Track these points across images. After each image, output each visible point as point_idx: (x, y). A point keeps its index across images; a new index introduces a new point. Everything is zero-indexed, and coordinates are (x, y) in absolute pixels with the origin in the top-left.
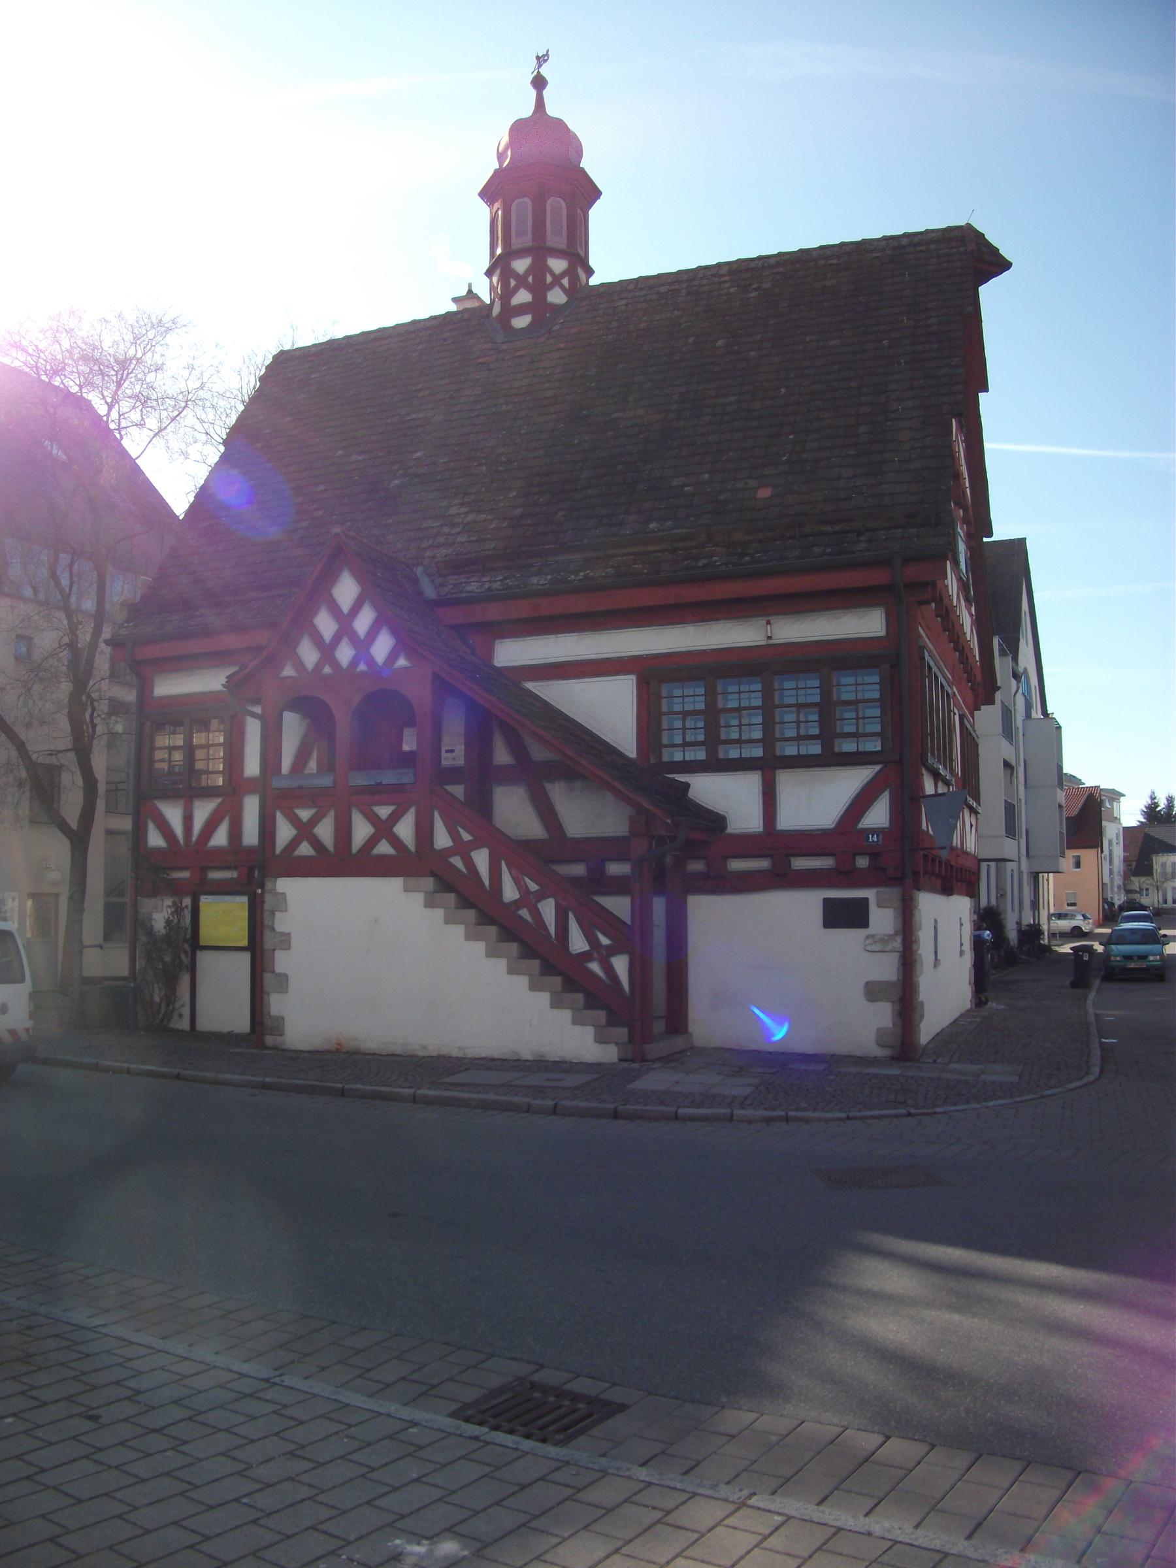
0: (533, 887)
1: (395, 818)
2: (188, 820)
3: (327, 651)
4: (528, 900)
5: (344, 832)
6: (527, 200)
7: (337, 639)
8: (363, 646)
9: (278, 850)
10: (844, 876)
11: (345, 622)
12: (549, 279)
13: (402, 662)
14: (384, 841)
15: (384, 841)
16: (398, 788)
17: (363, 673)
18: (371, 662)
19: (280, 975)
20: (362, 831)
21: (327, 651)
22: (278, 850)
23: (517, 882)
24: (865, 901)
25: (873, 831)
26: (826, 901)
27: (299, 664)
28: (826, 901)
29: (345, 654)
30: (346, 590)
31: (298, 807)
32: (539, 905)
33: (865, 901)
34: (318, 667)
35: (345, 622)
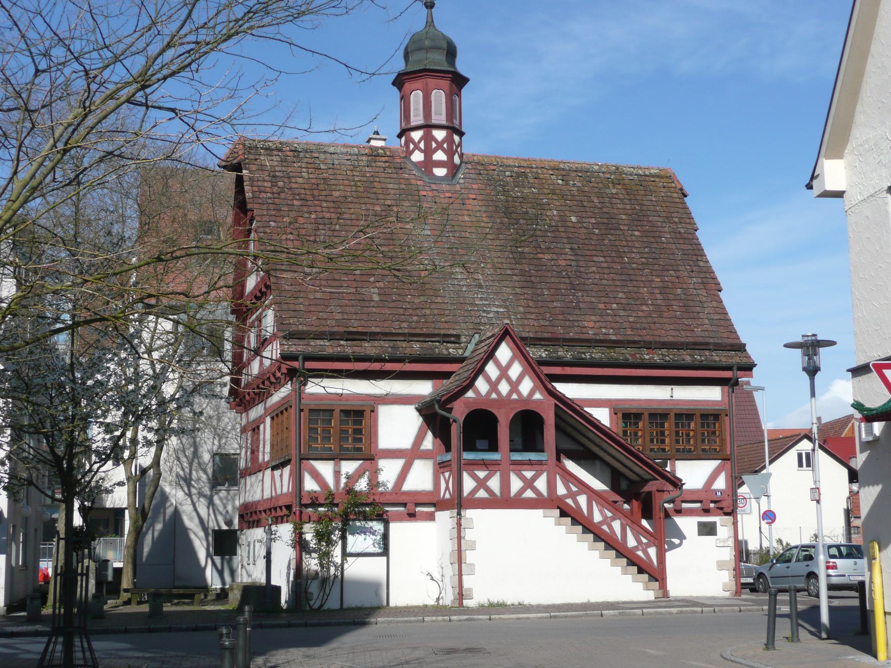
0: (609, 514)
1: (535, 478)
2: (337, 474)
3: (494, 386)
4: (606, 521)
5: (505, 484)
6: (419, 91)
7: (499, 380)
8: (514, 386)
9: (512, 494)
10: (706, 511)
11: (504, 372)
12: (434, 145)
13: (538, 396)
14: (529, 490)
15: (529, 490)
16: (540, 463)
17: (515, 400)
18: (519, 394)
19: (470, 564)
20: (516, 484)
21: (494, 386)
22: (512, 494)
23: (601, 512)
24: (715, 523)
25: (719, 490)
26: (699, 524)
27: (477, 392)
28: (699, 524)
29: (504, 388)
30: (504, 353)
31: (882, 490)
32: (612, 523)
33: (715, 523)
34: (489, 394)
35: (504, 372)
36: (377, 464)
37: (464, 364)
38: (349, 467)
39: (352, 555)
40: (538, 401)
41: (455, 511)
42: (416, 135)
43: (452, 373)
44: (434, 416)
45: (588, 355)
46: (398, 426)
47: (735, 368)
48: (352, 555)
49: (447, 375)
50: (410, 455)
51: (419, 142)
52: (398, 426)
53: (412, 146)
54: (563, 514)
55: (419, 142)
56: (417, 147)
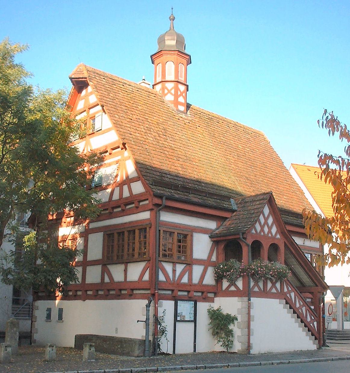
2: (174, 271)
12: (179, 93)
13: (278, 236)
23: (302, 311)
29: (266, 229)
36: (192, 267)
37: (235, 214)
38: (180, 268)
39: (192, 321)
40: (278, 239)
41: (247, 298)
42: (170, 86)
43: (226, 218)
44: (217, 240)
45: (192, 197)
46: (201, 247)
47: (164, 198)
48: (192, 321)
49: (225, 219)
50: (206, 263)
51: (171, 90)
52: (201, 247)
53: (166, 91)
54: (291, 308)
55: (171, 90)
56: (169, 92)
